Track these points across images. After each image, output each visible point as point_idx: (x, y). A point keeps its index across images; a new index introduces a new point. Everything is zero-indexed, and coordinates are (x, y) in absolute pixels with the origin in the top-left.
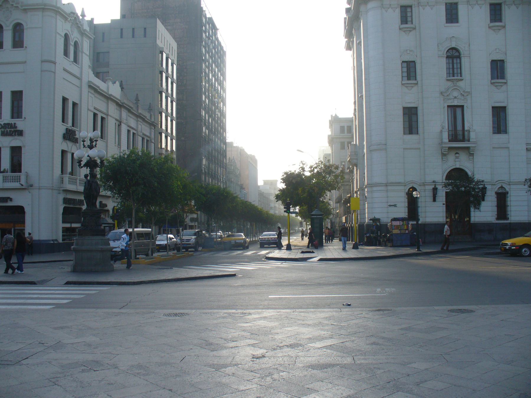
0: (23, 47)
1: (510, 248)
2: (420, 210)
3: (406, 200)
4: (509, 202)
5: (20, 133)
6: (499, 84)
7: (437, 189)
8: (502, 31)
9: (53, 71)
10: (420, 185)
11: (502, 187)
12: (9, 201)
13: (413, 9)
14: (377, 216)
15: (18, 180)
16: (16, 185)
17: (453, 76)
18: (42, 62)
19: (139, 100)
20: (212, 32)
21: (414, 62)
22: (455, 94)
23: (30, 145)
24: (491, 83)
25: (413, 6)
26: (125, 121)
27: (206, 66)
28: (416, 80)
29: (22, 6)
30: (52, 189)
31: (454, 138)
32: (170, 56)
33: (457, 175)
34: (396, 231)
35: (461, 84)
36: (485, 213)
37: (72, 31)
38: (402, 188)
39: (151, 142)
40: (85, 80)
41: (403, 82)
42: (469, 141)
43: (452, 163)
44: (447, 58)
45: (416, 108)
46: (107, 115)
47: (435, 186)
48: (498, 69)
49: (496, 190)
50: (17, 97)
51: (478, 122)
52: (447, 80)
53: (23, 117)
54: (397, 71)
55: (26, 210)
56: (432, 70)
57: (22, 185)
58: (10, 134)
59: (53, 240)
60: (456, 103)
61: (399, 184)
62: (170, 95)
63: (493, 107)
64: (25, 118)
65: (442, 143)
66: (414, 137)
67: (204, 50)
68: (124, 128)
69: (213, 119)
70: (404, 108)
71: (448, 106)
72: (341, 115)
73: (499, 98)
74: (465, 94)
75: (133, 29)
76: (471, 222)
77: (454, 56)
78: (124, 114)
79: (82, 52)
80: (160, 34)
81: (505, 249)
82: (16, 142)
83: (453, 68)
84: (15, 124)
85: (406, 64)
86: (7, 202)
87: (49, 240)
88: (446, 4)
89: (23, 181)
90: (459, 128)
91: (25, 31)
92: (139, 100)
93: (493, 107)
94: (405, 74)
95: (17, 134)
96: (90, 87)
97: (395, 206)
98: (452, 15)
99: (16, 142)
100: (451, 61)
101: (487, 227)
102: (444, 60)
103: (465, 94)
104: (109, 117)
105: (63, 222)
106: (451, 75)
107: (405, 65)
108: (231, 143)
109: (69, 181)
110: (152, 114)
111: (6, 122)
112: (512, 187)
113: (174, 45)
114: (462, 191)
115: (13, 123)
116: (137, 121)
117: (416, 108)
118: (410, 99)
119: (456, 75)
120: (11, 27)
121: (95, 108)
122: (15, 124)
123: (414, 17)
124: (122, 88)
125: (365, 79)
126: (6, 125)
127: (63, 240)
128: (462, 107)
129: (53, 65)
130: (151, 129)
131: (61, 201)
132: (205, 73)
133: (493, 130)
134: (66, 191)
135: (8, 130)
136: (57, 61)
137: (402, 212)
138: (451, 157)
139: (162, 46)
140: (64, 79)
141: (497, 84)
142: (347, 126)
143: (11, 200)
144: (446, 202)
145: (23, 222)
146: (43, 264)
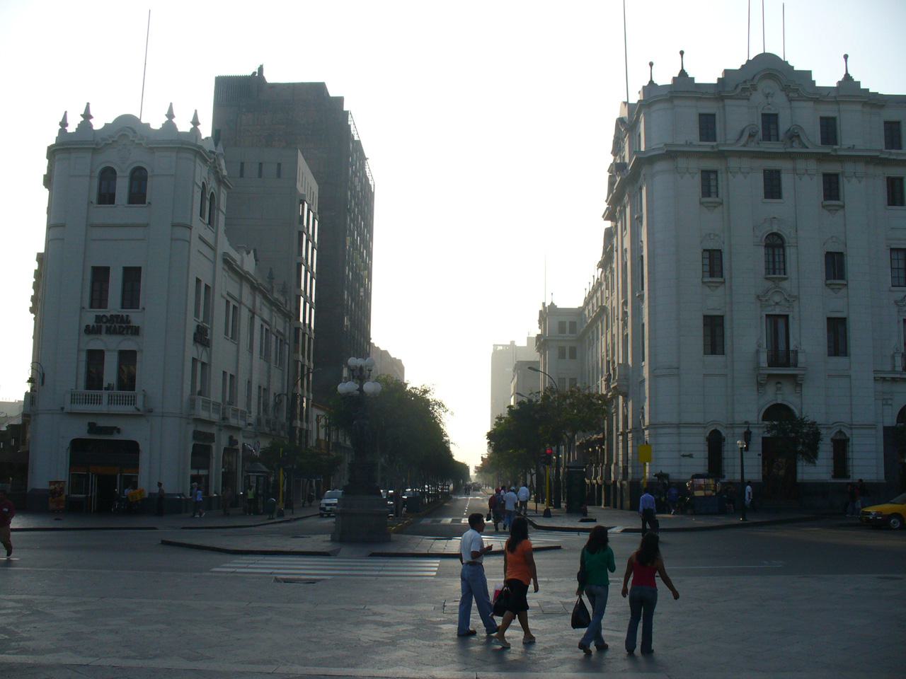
0: (145, 203)
1: (875, 519)
2: (725, 462)
3: (707, 448)
4: (850, 454)
5: (136, 331)
6: (838, 287)
7: (751, 432)
8: (840, 212)
10: (726, 427)
11: (840, 432)
12: (115, 432)
13: (719, 175)
14: (665, 471)
15: (132, 401)
16: (129, 409)
17: (774, 273)
18: (174, 225)
20: (359, 163)
21: (720, 250)
22: (777, 298)
24: (826, 285)
25: (719, 172)
27: (351, 219)
28: (722, 277)
31: (773, 362)
32: (312, 208)
33: (778, 413)
34: (699, 493)
35: (785, 284)
36: (817, 471)
38: (701, 430)
39: (286, 343)
40: (220, 252)
41: (706, 280)
42: (796, 365)
43: (772, 396)
44: (765, 246)
45: (722, 317)
46: (240, 303)
47: (748, 429)
48: (835, 265)
49: (832, 435)
50: (132, 276)
51: (809, 339)
52: (767, 279)
53: (140, 307)
54: (696, 263)
55: (141, 448)
56: (747, 262)
57: (139, 410)
59: (179, 495)
60: (777, 311)
61: (696, 425)
63: (829, 319)
64: (144, 309)
65: (758, 367)
66: (719, 358)
67: (349, 193)
70: (706, 317)
71: (767, 315)
72: (561, 304)
73: (836, 305)
74: (791, 300)
76: (798, 481)
77: (775, 245)
78: (259, 299)
79: (219, 209)
81: (868, 520)
82: (128, 344)
83: (774, 262)
84: (127, 316)
85: (708, 253)
86: (111, 433)
87: (174, 494)
88: (764, 171)
89: (139, 403)
90: (782, 347)
92: (273, 279)
93: (829, 319)
94: (707, 268)
95: (130, 332)
96: (226, 261)
97: (690, 456)
98: (773, 188)
99: (128, 344)
100: (771, 252)
101: (818, 489)
102: (762, 251)
103: (791, 300)
105: (193, 467)
106: (771, 271)
107: (707, 254)
108: (373, 344)
111: (114, 313)
112: (855, 431)
114: (787, 436)
115: (125, 314)
117: (722, 317)
118: (714, 303)
119: (777, 271)
120: (128, 173)
123: (720, 187)
125: (649, 273)
126: (115, 318)
128: (786, 317)
130: (285, 322)
132: (350, 230)
133: (829, 351)
134: (199, 421)
135: (117, 325)
137: (700, 463)
138: (771, 389)
139: (303, 193)
141: (833, 286)
142: (570, 322)
143: (119, 431)
144: (763, 452)
145: (136, 466)
146: (210, 530)
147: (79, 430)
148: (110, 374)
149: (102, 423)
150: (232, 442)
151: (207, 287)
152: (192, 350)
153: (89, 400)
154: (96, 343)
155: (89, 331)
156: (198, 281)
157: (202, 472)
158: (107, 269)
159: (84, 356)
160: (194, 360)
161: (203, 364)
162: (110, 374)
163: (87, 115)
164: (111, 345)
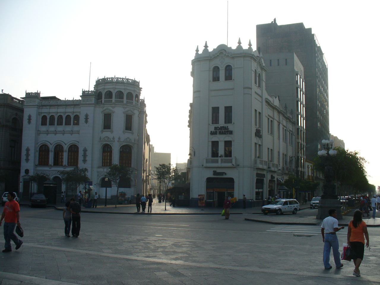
0: (232, 80)
5: (231, 133)
9: (250, 93)
15: (231, 161)
16: (229, 165)
19: (287, 108)
23: (237, 139)
26: (281, 122)
29: (231, 56)
30: (251, 168)
37: (257, 68)
40: (264, 98)
46: (274, 119)
50: (228, 110)
57: (233, 165)
58: (224, 133)
59: (251, 200)
62: (302, 103)
64: (234, 123)
67: (317, 70)
68: (281, 126)
69: (323, 117)
75: (271, 60)
80: (296, 62)
82: (228, 138)
84: (227, 127)
86: (223, 175)
91: (233, 70)
95: (229, 133)
96: (266, 102)
99: (228, 138)
104: (275, 120)
109: (260, 162)
110: (293, 116)
113: (302, 68)
115: (226, 126)
116: (287, 122)
121: (268, 115)
122: (227, 127)
124: (279, 101)
126: (222, 128)
127: (256, 199)
129: (251, 90)
130: (293, 126)
131: (255, 176)
134: (258, 169)
135: (223, 131)
136: (253, 87)
140: (255, 98)
143: (225, 174)
145: (233, 188)
147: (210, 174)
148: (221, 151)
149: (219, 171)
150: (272, 177)
151: (260, 113)
152: (255, 140)
153: (213, 162)
154: (215, 138)
155: (212, 133)
156: (256, 110)
157: (260, 190)
158: (217, 108)
159: (210, 144)
160: (256, 144)
161: (259, 145)
162: (221, 151)
163: (206, 46)
164: (221, 139)
